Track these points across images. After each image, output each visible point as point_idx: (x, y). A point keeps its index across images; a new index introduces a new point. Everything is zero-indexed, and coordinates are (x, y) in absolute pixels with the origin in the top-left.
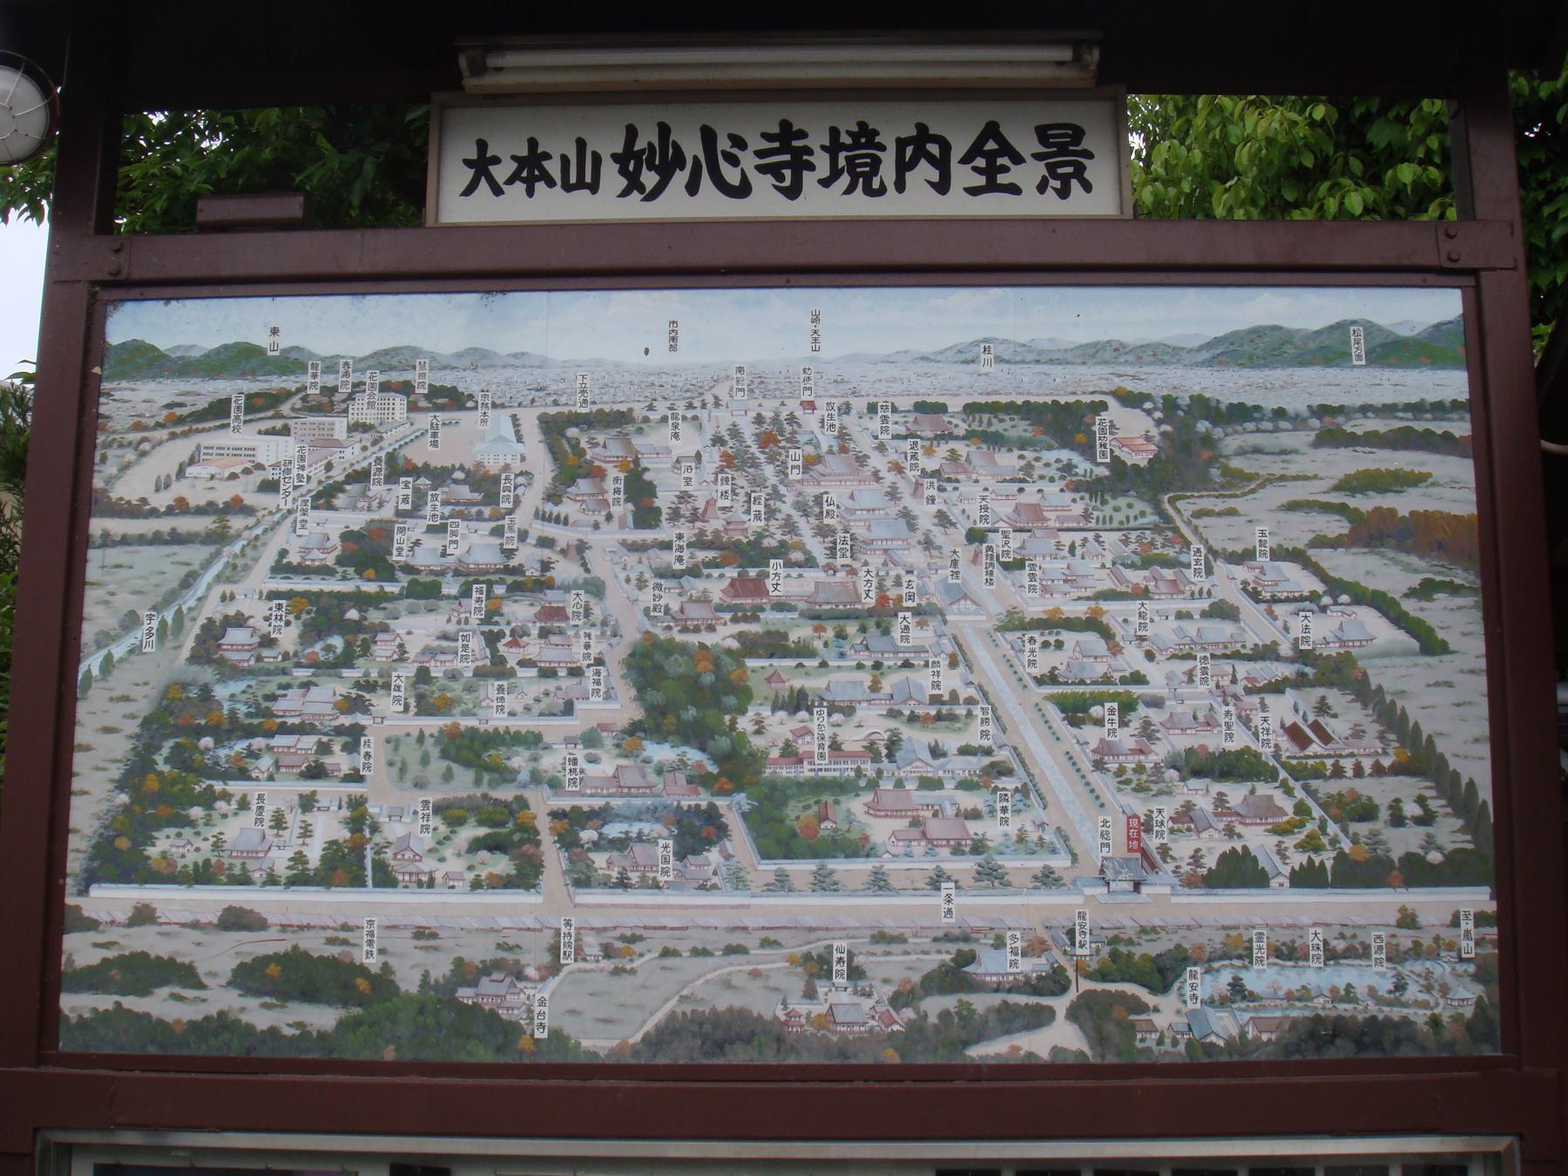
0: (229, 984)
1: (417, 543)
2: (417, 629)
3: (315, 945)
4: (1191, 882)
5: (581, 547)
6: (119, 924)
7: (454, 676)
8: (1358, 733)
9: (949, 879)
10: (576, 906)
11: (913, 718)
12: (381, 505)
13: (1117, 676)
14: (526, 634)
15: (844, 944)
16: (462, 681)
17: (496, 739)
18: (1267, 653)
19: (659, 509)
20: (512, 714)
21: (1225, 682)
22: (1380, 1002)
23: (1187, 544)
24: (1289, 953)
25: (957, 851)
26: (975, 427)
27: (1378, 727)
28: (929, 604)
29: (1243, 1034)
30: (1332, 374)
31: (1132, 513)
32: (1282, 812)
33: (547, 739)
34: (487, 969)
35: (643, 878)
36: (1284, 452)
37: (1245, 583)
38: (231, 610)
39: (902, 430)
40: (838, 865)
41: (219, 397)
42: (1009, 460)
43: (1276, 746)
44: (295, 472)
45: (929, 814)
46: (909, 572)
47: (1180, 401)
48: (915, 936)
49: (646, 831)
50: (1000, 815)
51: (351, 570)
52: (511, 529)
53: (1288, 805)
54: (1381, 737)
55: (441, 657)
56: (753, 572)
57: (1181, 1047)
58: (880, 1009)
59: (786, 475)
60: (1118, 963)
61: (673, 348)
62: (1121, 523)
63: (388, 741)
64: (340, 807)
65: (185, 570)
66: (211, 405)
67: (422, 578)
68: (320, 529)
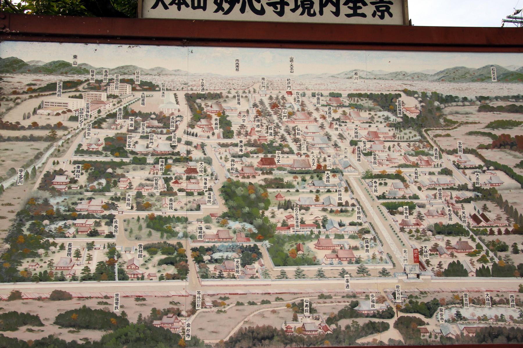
0: (54, 323)
1: (136, 142)
2: (137, 176)
3: (92, 304)
4: (439, 274)
5: (203, 146)
6: (4, 300)
7: (152, 195)
8: (499, 218)
9: (347, 273)
10: (202, 286)
11: (332, 211)
12: (121, 127)
13: (407, 196)
14: (181, 178)
15: (308, 299)
16: (156, 197)
17: (169, 219)
18: (463, 188)
19: (233, 131)
20: (176, 210)
21: (448, 198)
22: (515, 321)
23: (432, 147)
24: (477, 302)
25: (350, 262)
26: (352, 102)
27: (506, 216)
28: (336, 168)
29: (462, 334)
30: (484, 85)
31: (411, 135)
32: (471, 248)
33: (190, 220)
34: (167, 312)
35: (229, 274)
36: (467, 113)
37: (454, 162)
38: (57, 168)
39: (325, 103)
40: (305, 268)
41: (51, 82)
42: (365, 115)
43: (468, 222)
44: (85, 113)
45: (339, 248)
46: (329, 156)
47: (428, 94)
48: (335, 296)
49: (230, 256)
50: (366, 248)
51: (109, 153)
52: (174, 138)
53: (473, 245)
54: (508, 219)
55: (146, 188)
56: (269, 156)
57: (438, 339)
58: (323, 325)
59: (281, 119)
60: (413, 306)
61: (237, 70)
62: (407, 139)
63: (125, 221)
64: (104, 248)
65: (36, 152)
66: (48, 85)
67: (138, 156)
68: (96, 136)
